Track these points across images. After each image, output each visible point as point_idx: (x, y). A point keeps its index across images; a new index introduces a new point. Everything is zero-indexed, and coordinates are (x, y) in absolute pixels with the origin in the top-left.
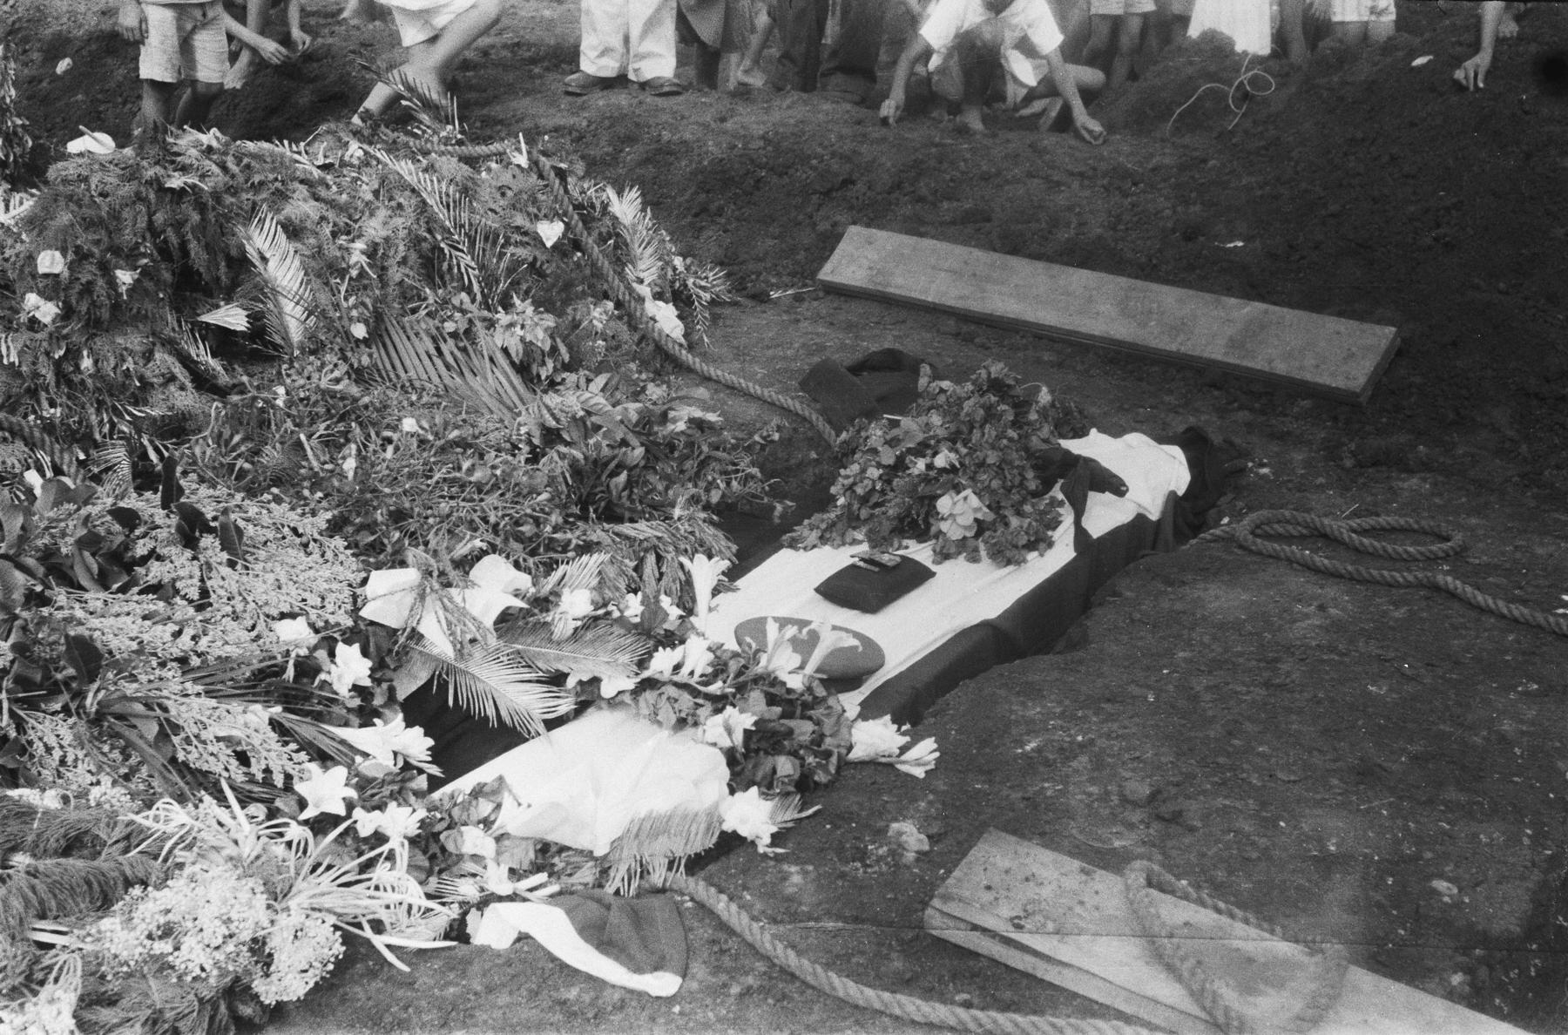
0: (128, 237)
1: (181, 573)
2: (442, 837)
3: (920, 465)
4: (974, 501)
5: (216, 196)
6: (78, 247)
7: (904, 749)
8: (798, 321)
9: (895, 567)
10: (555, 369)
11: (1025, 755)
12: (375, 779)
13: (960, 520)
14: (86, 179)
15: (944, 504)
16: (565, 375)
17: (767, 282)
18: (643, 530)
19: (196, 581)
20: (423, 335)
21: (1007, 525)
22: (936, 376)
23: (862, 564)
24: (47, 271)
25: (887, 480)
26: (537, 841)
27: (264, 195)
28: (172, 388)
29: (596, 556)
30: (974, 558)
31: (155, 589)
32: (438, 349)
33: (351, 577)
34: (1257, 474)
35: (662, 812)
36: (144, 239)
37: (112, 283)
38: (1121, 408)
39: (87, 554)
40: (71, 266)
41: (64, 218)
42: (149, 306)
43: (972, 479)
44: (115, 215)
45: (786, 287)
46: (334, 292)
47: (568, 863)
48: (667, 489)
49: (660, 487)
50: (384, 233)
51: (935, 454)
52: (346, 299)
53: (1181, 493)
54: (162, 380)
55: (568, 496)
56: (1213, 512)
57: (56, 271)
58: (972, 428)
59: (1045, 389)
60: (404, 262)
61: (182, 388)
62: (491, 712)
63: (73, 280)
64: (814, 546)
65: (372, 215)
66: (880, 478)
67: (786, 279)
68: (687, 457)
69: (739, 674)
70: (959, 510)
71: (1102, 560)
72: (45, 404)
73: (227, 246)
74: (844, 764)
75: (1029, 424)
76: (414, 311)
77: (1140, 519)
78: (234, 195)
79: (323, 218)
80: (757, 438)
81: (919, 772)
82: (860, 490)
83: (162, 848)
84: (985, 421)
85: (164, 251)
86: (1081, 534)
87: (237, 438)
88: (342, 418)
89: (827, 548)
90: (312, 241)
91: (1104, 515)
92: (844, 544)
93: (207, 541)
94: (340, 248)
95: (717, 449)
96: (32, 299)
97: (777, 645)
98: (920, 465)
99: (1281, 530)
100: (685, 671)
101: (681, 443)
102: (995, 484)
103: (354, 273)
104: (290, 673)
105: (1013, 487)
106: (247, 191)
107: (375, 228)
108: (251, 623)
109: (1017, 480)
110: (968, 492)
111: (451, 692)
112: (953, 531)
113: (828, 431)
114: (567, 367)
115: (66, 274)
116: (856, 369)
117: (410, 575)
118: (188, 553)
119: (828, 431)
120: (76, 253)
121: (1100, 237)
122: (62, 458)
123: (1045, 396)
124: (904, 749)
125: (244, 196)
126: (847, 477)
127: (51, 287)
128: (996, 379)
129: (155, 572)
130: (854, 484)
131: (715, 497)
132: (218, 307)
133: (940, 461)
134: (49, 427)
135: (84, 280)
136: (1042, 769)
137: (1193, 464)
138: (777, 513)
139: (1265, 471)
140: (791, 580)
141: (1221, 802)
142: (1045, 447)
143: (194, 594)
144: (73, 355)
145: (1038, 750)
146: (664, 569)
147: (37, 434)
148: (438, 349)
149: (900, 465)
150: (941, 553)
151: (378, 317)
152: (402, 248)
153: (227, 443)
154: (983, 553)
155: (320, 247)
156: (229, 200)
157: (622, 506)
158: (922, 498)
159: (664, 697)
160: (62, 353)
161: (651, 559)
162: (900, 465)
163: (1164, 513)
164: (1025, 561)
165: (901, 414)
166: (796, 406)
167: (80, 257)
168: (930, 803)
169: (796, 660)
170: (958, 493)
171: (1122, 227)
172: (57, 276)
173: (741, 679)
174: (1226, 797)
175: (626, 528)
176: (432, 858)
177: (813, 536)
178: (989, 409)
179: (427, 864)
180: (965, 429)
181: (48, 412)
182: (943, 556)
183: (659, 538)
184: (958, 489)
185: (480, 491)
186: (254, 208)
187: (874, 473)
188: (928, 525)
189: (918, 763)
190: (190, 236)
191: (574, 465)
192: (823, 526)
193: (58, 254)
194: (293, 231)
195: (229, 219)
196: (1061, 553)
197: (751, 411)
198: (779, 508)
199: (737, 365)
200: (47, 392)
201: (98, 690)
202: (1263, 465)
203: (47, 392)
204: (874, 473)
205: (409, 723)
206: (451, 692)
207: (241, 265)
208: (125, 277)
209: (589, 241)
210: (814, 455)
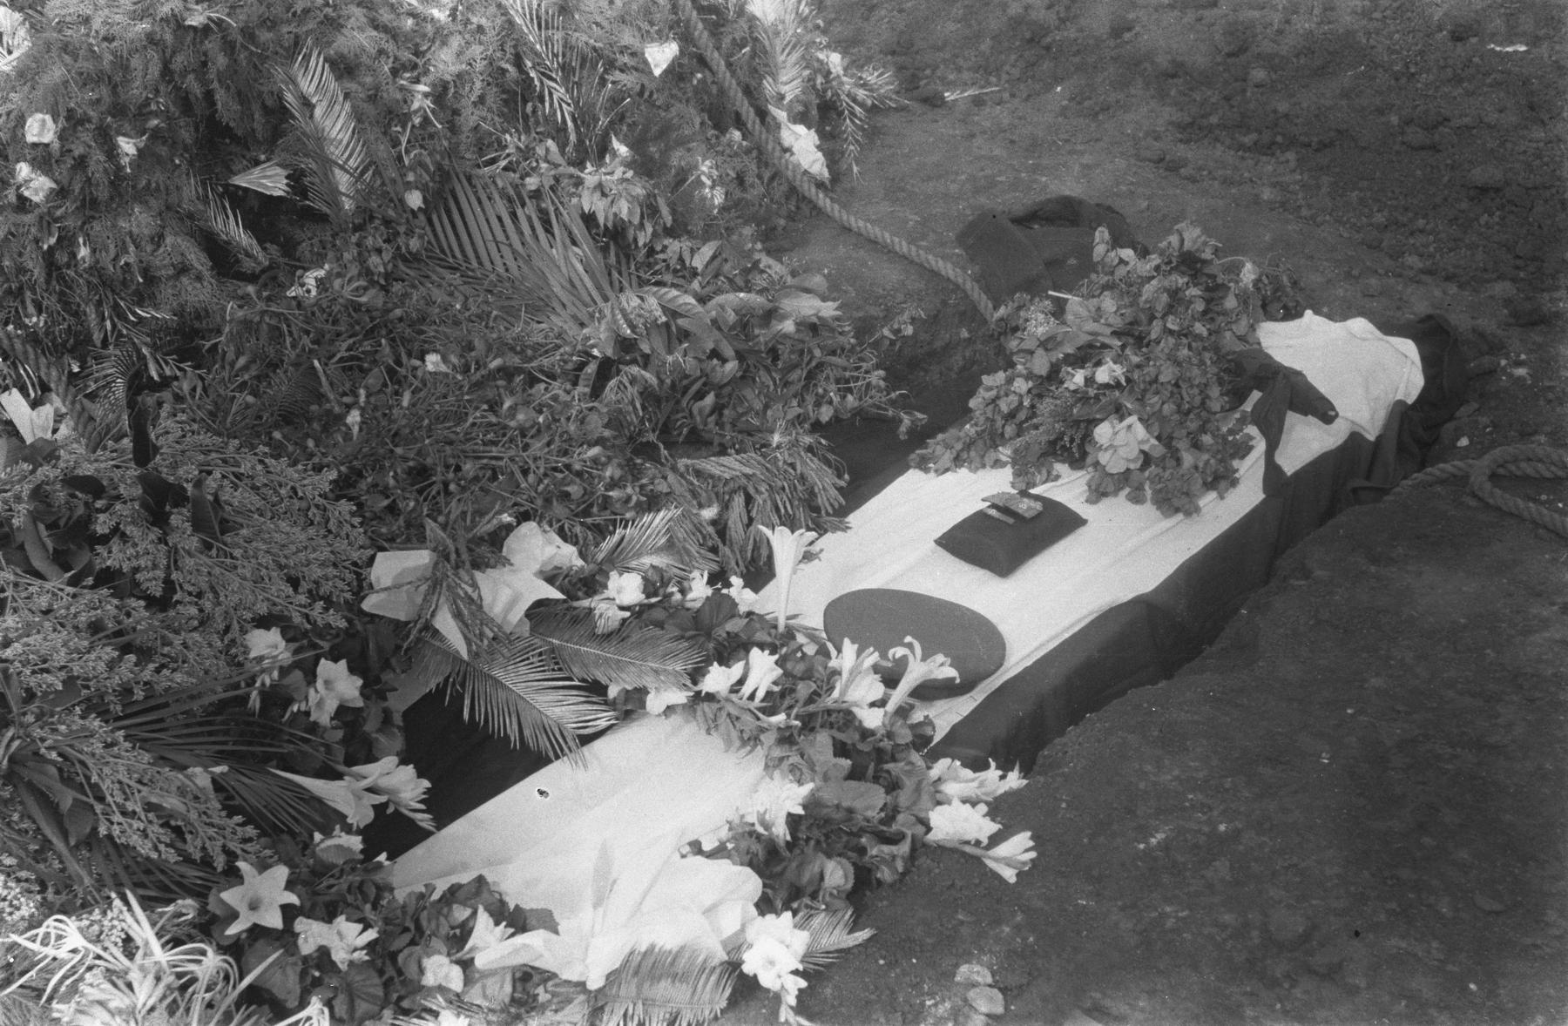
0: (136, 91)
1: (142, 562)
2: (401, 958)
3: (1079, 378)
4: (1140, 431)
5: (248, 33)
6: (70, 111)
7: (995, 840)
8: (973, 136)
9: (1033, 518)
10: (655, 234)
11: (1148, 853)
12: (334, 866)
13: (1122, 452)
14: (86, 20)
15: (1103, 432)
16: (666, 242)
17: (943, 79)
18: (728, 466)
19: (160, 574)
20: (496, 196)
21: (1179, 461)
22: (1116, 242)
23: (993, 512)
24: (35, 139)
25: (1038, 394)
26: (514, 969)
27: (311, 25)
28: (185, 280)
29: (662, 514)
30: (1136, 499)
31: (107, 577)
32: (514, 215)
33: (355, 556)
34: (1511, 376)
35: (668, 947)
36: (157, 91)
37: (112, 152)
38: (1348, 275)
39: (41, 527)
40: (62, 136)
41: (56, 73)
42: (159, 177)
43: (1141, 400)
44: (122, 64)
45: (965, 86)
46: (396, 143)
47: (554, 995)
48: (767, 407)
49: (758, 406)
50: (455, 69)
51: (1099, 364)
52: (407, 152)
53: (1410, 401)
54: (171, 272)
55: (642, 422)
56: (1450, 426)
57: (46, 140)
58: (1152, 318)
59: (1249, 266)
60: (482, 100)
61: (199, 278)
62: (514, 734)
63: (66, 152)
64: (947, 470)
65: (444, 43)
66: (1029, 391)
67: (966, 75)
68: (795, 367)
69: (810, 700)
70: (1122, 439)
71: (1300, 504)
72: (31, 309)
73: (260, 94)
74: (920, 848)
75: (1225, 313)
76: (493, 161)
77: (1355, 438)
78: (269, 29)
79: (381, 52)
80: (886, 332)
81: (1009, 875)
82: (1004, 406)
83: (49, 980)
84: (1170, 310)
85: (185, 102)
86: (1272, 470)
87: (242, 361)
88: (370, 333)
89: (964, 471)
90: (368, 80)
91: (1305, 443)
92: (984, 466)
93: (179, 518)
94: (402, 88)
95: (833, 353)
96: (23, 170)
97: (855, 672)
98: (1079, 378)
99: (1530, 471)
100: (746, 690)
101: (784, 351)
102: (1168, 408)
103: (417, 121)
104: (255, 700)
105: (1189, 412)
106: (289, 22)
107: (445, 62)
108: (222, 627)
109: (1198, 400)
110: (1133, 419)
111: (467, 702)
112: (1114, 463)
113: (984, 303)
114: (670, 232)
115: (56, 145)
116: (1026, 220)
117: (421, 558)
118: (155, 533)
119: (984, 303)
120: (68, 119)
121: (1350, 33)
122: (48, 374)
123: (1248, 273)
124: (995, 840)
125: (285, 29)
126: (990, 389)
127: (43, 158)
128: (1189, 253)
129: (114, 557)
130: (998, 397)
131: (826, 414)
132: (257, 163)
133: (1103, 375)
134: (33, 338)
135: (76, 153)
136: (1165, 879)
137: (1430, 364)
138: (903, 429)
139: (1521, 372)
140: (905, 529)
141: (1395, 943)
142: (1239, 347)
143: (156, 590)
144: (67, 241)
145: (1165, 846)
146: (754, 514)
147: (18, 346)
148: (514, 215)
149: (1055, 375)
150: (1096, 490)
151: (444, 175)
152: (478, 84)
153: (232, 364)
154: (1149, 493)
155: (377, 88)
156: (265, 36)
157: (710, 432)
158: (1077, 423)
159: (724, 714)
160: (53, 241)
161: (739, 500)
162: (1055, 375)
163: (1387, 427)
164: (1197, 510)
165: (1070, 291)
166: (948, 269)
167: (72, 123)
168: (1017, 928)
169: (878, 690)
170: (1121, 419)
171: (1377, 15)
172: (47, 145)
173: (811, 708)
174: (1403, 937)
175: (712, 465)
176: (387, 985)
177: (947, 457)
178: (1174, 294)
179: (380, 992)
180: (1143, 318)
181: (34, 320)
182: (1098, 493)
183: (747, 476)
184: (1120, 412)
185: (524, 436)
186: (297, 43)
187: (1021, 385)
188: (1084, 455)
189: (1008, 862)
190: (215, 85)
191: (647, 394)
192: (959, 446)
193: (48, 118)
194: (344, 68)
195: (264, 58)
196: (1247, 495)
197: (889, 275)
198: (907, 421)
199: (885, 207)
200: (34, 292)
201: (12, 739)
202: (1519, 364)
203: (34, 292)
204: (1021, 385)
205: (404, 762)
206: (467, 702)
207: (278, 114)
208: (128, 146)
209: (717, 60)
210: (965, 334)
